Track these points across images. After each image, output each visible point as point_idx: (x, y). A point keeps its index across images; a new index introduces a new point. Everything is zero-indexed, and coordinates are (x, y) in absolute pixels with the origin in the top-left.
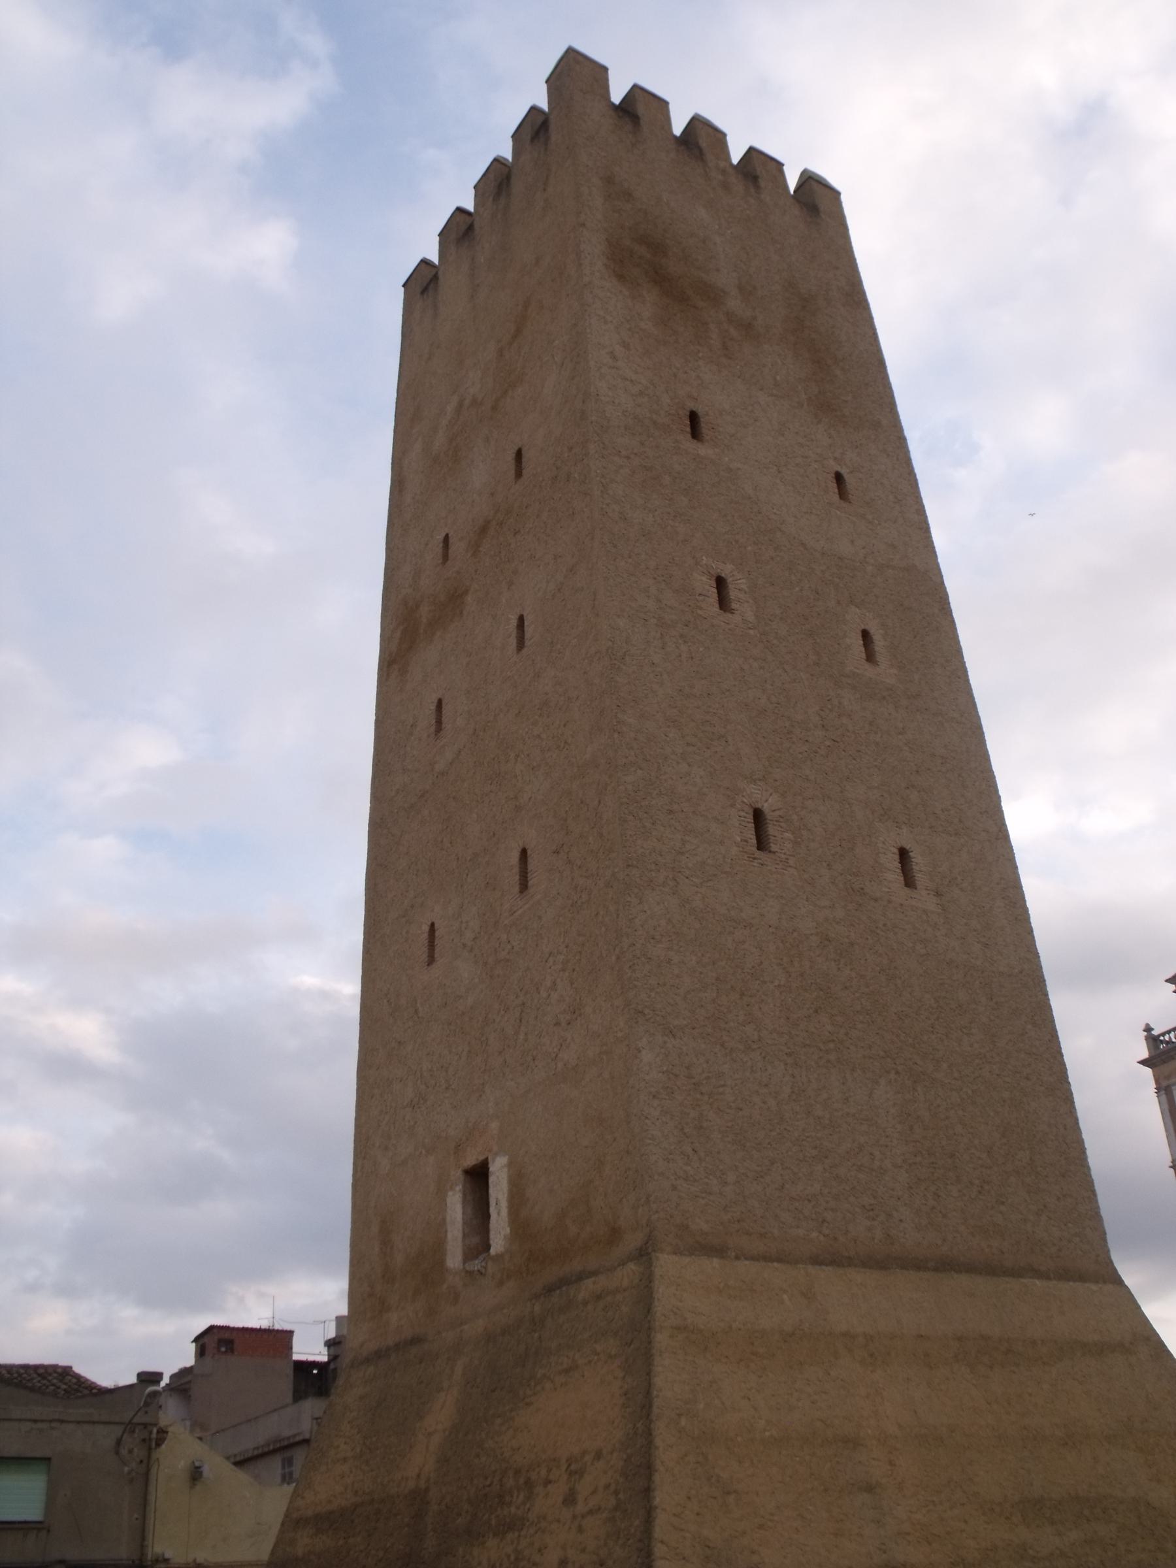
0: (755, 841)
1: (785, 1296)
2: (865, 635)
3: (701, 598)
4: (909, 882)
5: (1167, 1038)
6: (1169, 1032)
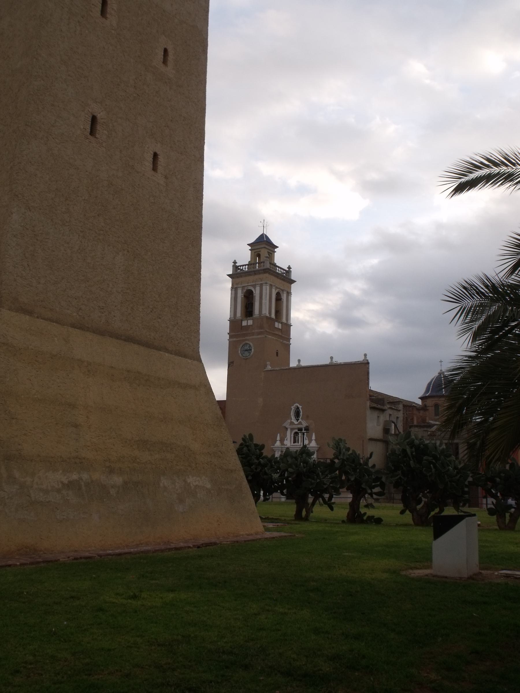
0: (89, 130)
1: (56, 339)
2: (166, 51)
3: (93, 6)
4: (155, 168)
5: (241, 268)
6: (243, 266)
